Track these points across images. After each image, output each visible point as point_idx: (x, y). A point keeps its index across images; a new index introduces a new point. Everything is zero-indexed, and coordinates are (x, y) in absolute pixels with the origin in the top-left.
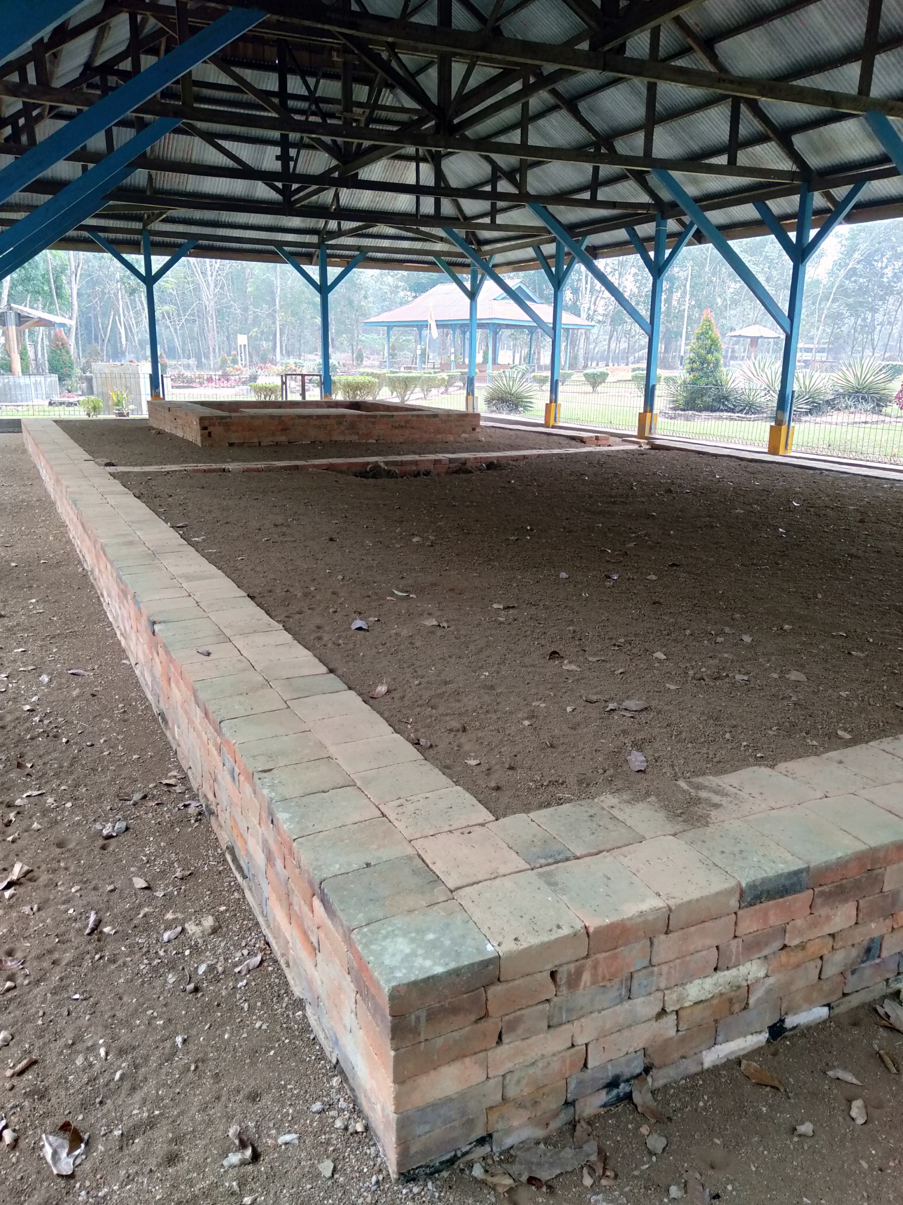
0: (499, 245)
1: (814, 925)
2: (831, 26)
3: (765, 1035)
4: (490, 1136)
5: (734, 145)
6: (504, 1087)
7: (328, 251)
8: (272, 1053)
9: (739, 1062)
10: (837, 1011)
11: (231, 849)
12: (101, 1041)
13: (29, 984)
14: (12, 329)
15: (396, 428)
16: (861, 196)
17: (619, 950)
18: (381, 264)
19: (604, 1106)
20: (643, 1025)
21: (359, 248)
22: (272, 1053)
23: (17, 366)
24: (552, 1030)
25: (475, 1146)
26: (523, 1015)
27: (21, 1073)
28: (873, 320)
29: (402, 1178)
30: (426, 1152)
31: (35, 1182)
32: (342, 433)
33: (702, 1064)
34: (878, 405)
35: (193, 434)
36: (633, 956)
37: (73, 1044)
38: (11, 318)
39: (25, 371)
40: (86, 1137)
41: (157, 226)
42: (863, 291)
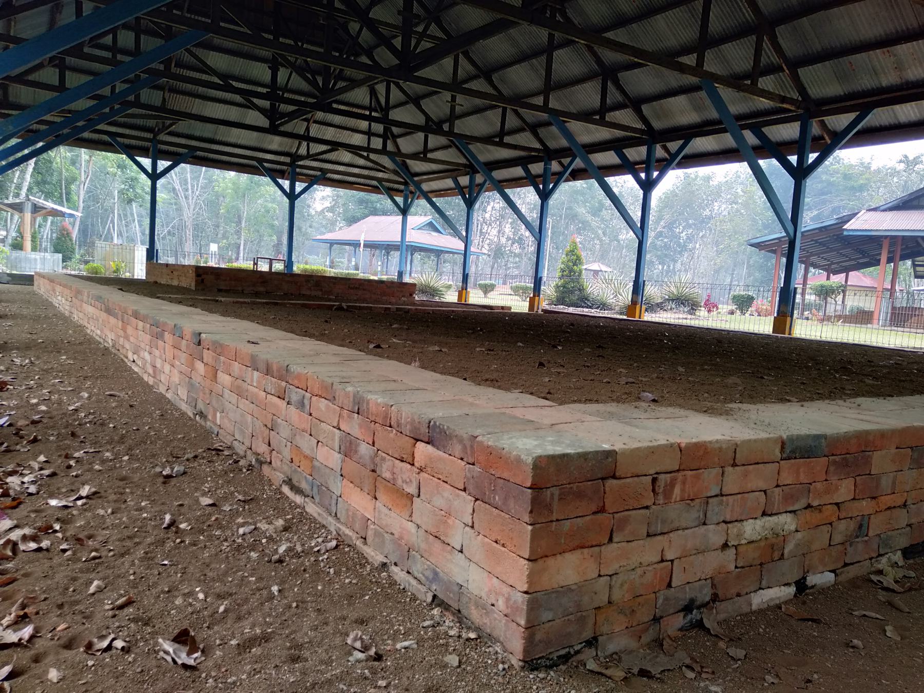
0: (425, 177)
1: (827, 491)
3: (792, 590)
4: (595, 638)
5: (604, 109)
6: (610, 587)
7: (298, 170)
8: (367, 597)
10: (840, 579)
11: (289, 482)
12: (197, 589)
13: (113, 556)
14: (28, 216)
15: (352, 288)
17: (701, 471)
18: (336, 184)
19: (681, 630)
20: (713, 553)
21: (321, 170)
22: (367, 597)
23: (28, 244)
24: (649, 539)
25: (585, 646)
26: (630, 516)
27: (121, 607)
28: (674, 268)
29: (527, 665)
31: (156, 674)
32: (310, 289)
34: (693, 309)
35: (189, 282)
37: (169, 591)
38: (28, 207)
39: (34, 249)
40: (201, 646)
41: (163, 137)
42: (666, 247)
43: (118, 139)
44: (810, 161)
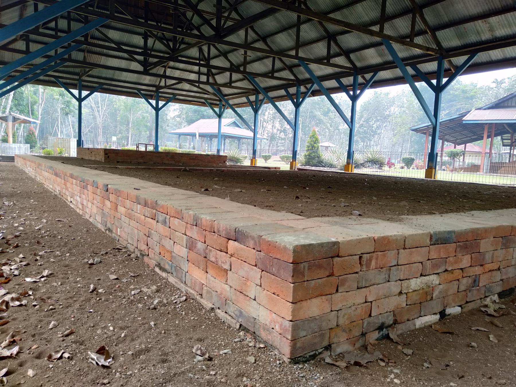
1: (456, 262)
2: (365, 12)
3: (438, 317)
5: (329, 56)
7: (160, 94)
8: (203, 327)
9: (431, 326)
10: (464, 310)
11: (159, 265)
14: (10, 123)
16: (375, 79)
17: (386, 252)
18: (181, 102)
19: (377, 340)
21: (173, 94)
23: (11, 139)
24: (358, 290)
25: (324, 350)
27: (67, 335)
28: (370, 144)
30: (303, 348)
31: (88, 371)
33: (415, 325)
36: (391, 257)
37: (93, 326)
38: (10, 119)
39: (14, 142)
40: (112, 355)
43: (60, 80)
44: (443, 83)
